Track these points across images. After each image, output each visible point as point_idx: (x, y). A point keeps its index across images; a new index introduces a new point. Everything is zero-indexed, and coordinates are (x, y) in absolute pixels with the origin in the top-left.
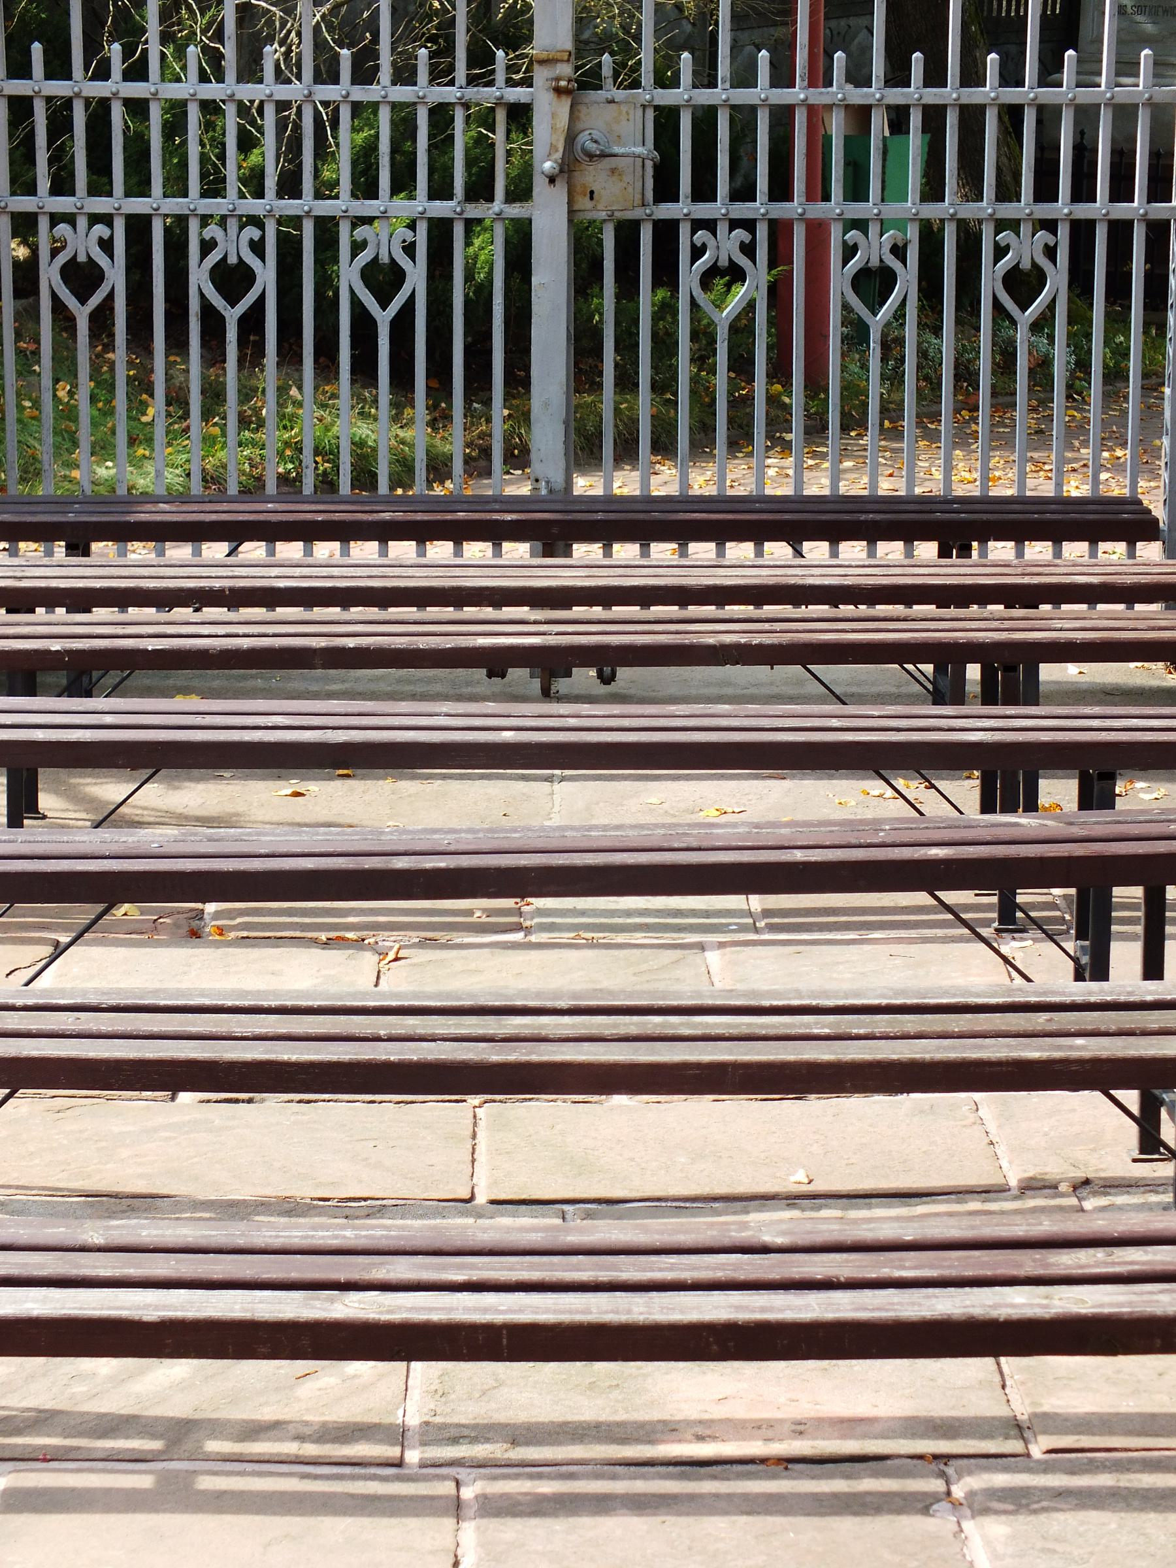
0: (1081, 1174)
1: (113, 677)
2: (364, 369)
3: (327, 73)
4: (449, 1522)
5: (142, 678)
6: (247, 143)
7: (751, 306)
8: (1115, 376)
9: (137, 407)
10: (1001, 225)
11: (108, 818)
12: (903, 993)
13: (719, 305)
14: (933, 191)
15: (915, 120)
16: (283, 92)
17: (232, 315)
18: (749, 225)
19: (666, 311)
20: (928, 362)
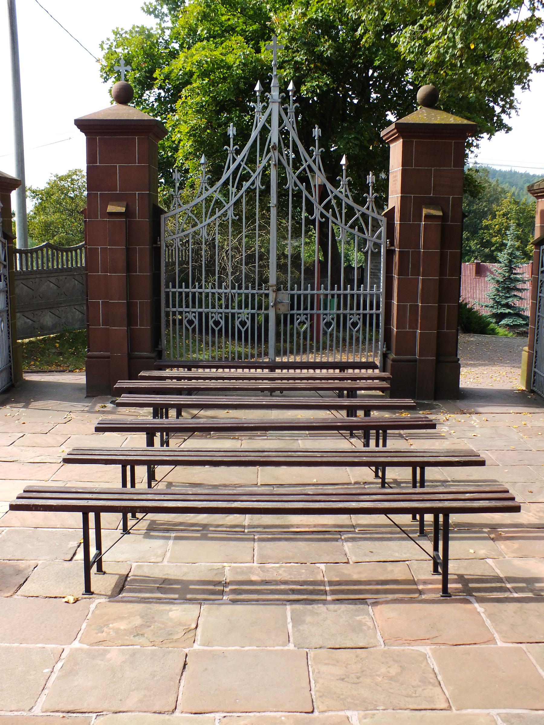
0: (364, 481)
1: (195, 392)
2: (240, 339)
3: (233, 288)
4: (253, 542)
5: (200, 392)
6: (220, 299)
7: (307, 328)
8: (370, 340)
9: (200, 345)
10: (351, 314)
11: (194, 417)
12: (333, 449)
13: (301, 328)
14: (339, 308)
15: (336, 296)
16: (226, 291)
17: (217, 329)
18: (307, 314)
19: (292, 329)
20: (338, 338)
